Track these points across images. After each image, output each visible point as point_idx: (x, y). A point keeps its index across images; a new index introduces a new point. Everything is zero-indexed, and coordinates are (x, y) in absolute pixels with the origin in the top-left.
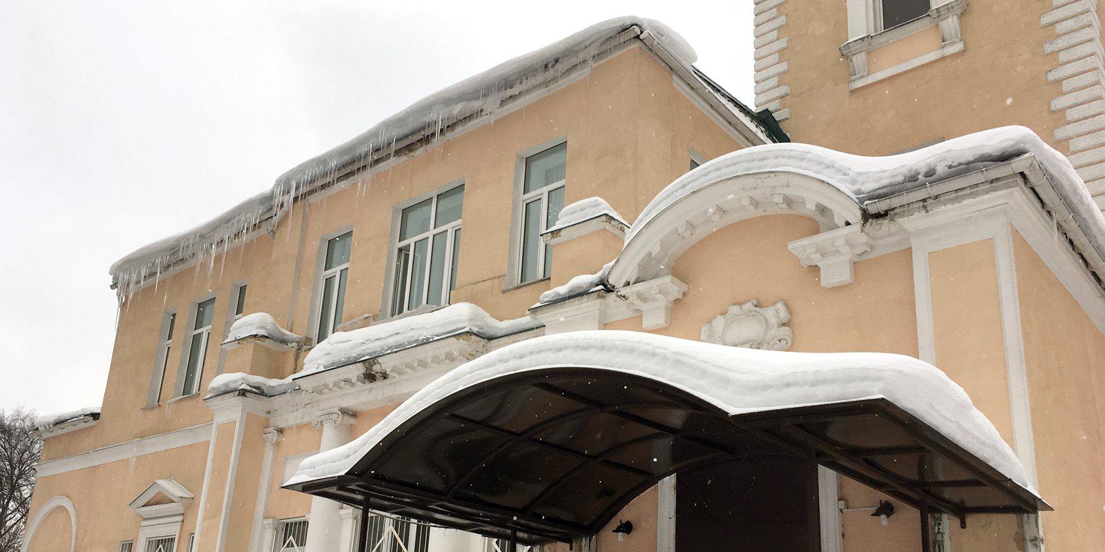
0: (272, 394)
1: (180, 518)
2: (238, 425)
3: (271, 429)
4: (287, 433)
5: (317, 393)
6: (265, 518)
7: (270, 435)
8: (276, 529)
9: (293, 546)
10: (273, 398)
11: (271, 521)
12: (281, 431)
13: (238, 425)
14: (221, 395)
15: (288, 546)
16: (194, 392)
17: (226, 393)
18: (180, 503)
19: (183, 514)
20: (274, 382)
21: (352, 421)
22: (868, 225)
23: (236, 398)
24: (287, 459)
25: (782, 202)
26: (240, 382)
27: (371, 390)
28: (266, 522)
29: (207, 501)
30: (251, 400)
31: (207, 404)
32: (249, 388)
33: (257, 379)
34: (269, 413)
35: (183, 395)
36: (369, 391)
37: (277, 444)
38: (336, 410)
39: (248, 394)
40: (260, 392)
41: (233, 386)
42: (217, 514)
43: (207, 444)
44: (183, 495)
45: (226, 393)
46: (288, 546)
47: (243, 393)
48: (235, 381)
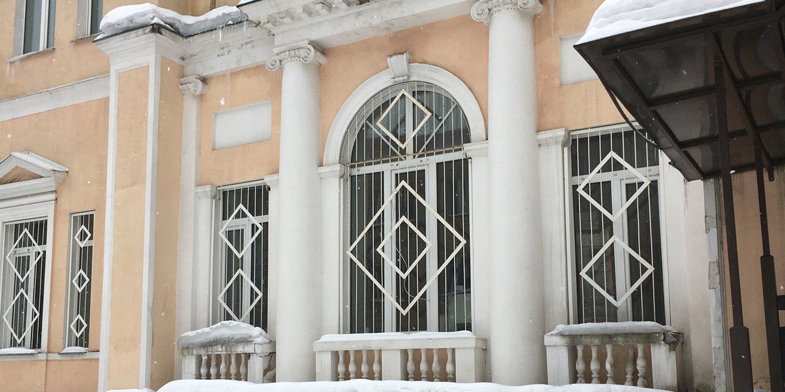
0: (189, 34)
1: (53, 196)
2: (152, 71)
3: (192, 78)
4: (213, 84)
5: (272, 24)
6: (199, 184)
7: (190, 86)
8: (214, 197)
9: (244, 216)
10: (191, 39)
11: (208, 188)
12: (204, 80)
13: (152, 71)
14: (122, 33)
15: (237, 216)
16: (41, 49)
17: (128, 30)
18: (53, 178)
19: (55, 191)
20: (189, 20)
21: (322, 60)
22: (326, 53)
23: (146, 35)
24: (216, 114)
25: (321, 8)
26: (151, 16)
27: (359, 14)
28: (200, 189)
29: (118, 166)
30: (165, 39)
31: (98, 46)
32: (162, 23)
33: (170, 14)
34: (183, 59)
35: (24, 54)
36: (357, 16)
37: (201, 97)
38: (305, 43)
39: (163, 31)
40: (175, 30)
41: (140, 21)
42: (137, 180)
43: (106, 101)
44: (55, 169)
45: (128, 30)
46: (237, 216)
47: (156, 29)
48: (144, 14)
